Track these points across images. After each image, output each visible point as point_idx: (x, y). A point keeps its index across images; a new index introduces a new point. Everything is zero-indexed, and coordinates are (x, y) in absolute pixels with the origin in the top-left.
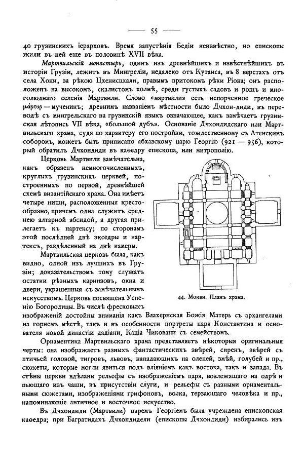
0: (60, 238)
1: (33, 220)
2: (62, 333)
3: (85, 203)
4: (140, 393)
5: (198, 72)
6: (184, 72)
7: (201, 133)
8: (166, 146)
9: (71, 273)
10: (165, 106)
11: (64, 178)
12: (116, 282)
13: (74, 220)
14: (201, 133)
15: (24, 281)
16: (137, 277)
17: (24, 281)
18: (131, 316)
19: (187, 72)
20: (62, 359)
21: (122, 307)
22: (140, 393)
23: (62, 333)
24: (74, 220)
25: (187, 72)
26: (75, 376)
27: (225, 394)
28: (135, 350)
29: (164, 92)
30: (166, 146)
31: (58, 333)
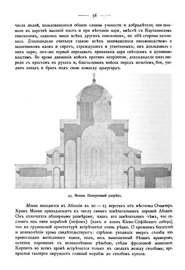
0: (141, 238)
1: (91, 243)
2: (51, 227)
3: (46, 26)
4: (132, 243)
5: (147, 31)
6: (128, 206)
7: (139, 249)
8: (140, 252)
9: (76, 233)
10: (140, 205)
11: (35, 228)
12: (80, 239)
13: (122, 254)
14: (139, 249)
15: (17, 47)
16: (19, 235)
17: (17, 47)
18: (71, 238)
19: (130, 206)
20: (116, 238)
21: (140, 243)
22: (132, 243)
23: (51, 227)
24: (122, 254)
25: (130, 206)
26: (66, 232)
27: (64, 238)
28: (132, 243)
29: (113, 207)
30: (140, 252)
31: (148, 243)
